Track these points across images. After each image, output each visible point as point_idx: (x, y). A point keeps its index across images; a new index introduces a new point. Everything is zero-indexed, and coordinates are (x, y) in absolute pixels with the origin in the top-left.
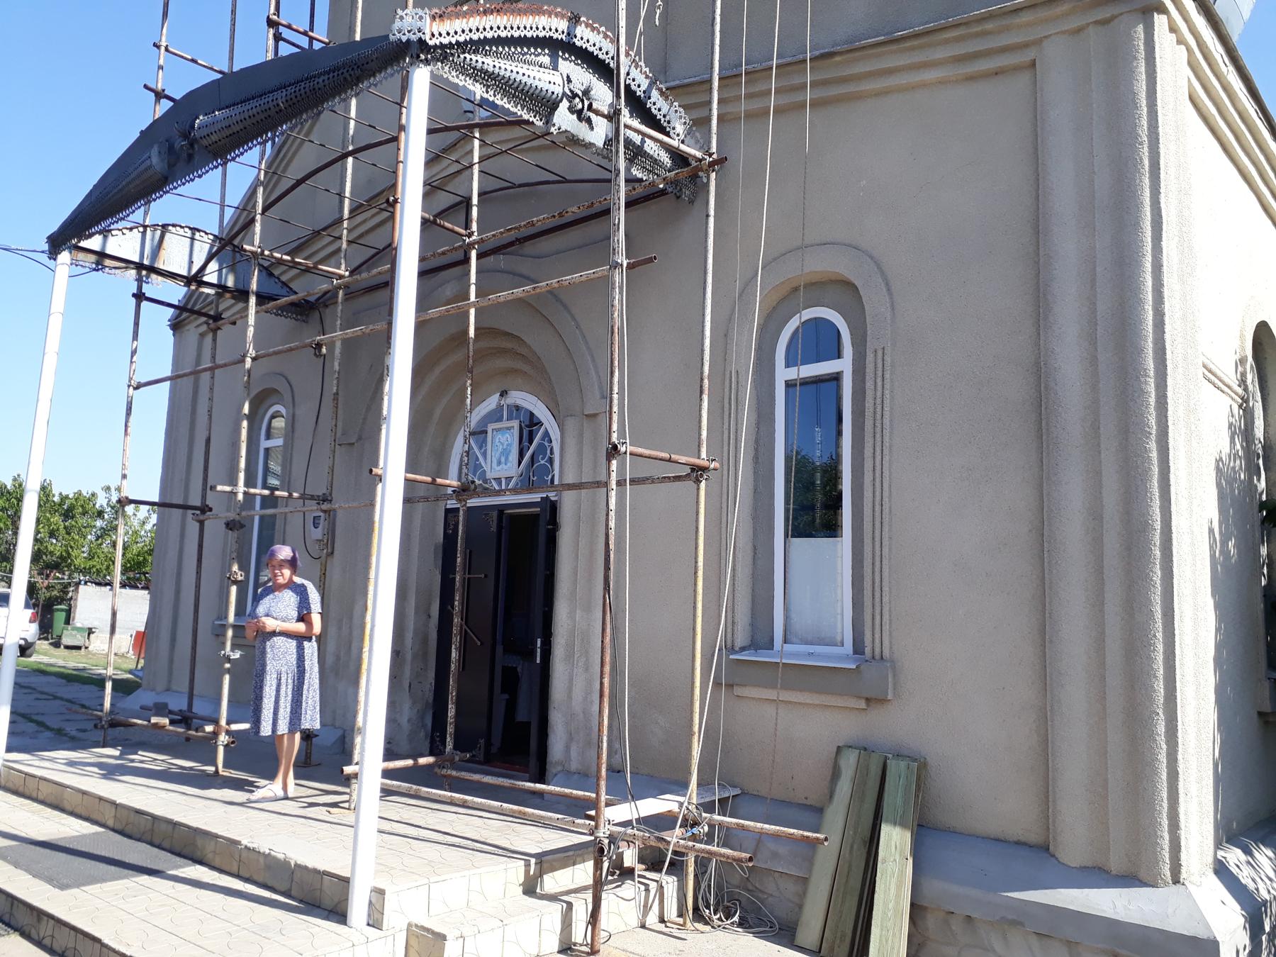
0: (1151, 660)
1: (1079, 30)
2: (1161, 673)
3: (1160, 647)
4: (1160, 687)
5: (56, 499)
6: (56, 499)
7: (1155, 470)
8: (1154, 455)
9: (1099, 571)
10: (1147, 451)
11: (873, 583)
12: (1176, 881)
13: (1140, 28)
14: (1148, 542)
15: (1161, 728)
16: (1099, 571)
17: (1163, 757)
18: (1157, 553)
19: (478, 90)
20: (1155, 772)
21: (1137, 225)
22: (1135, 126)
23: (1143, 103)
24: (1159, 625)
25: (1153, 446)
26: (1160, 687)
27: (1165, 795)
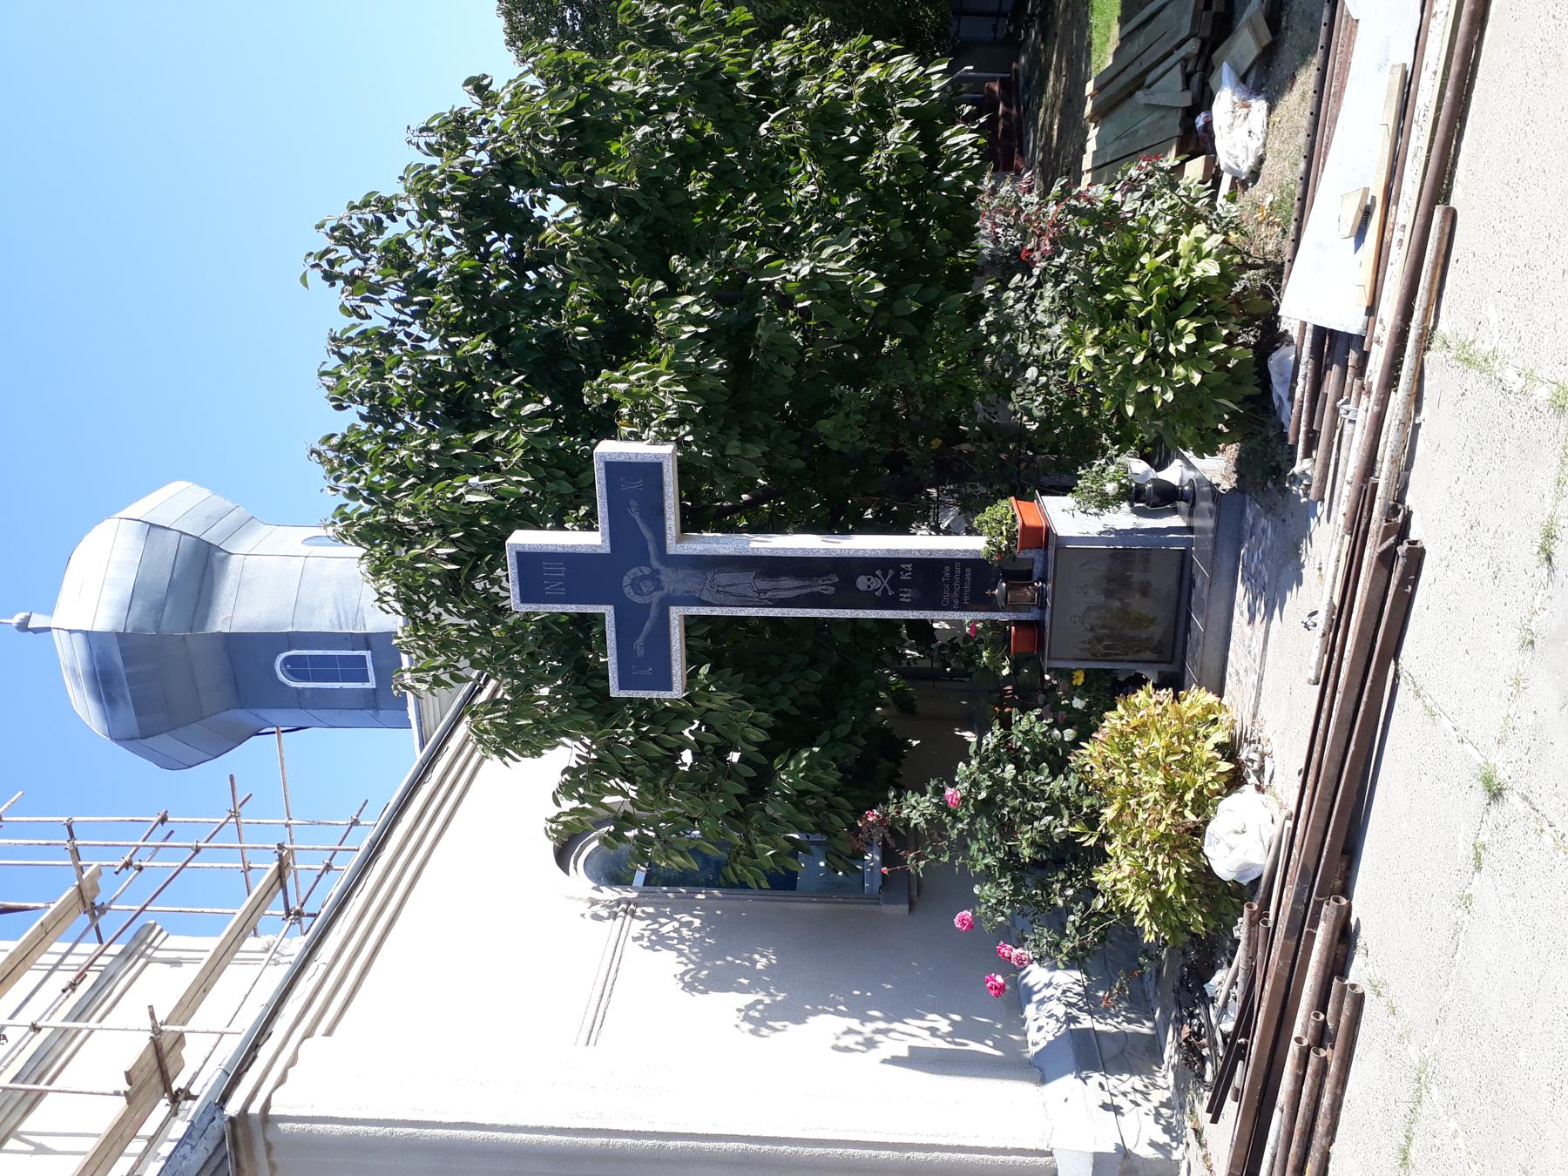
0: (861, 1158)
1: (273, 1166)
2: (873, 1153)
3: (850, 1151)
4: (884, 1154)
5: (353, 415)
6: (353, 415)
7: (693, 1144)
8: (679, 1143)
9: (1290, 1134)
10: (676, 1149)
11: (1339, 449)
12: (1050, 1154)
13: (281, 1126)
14: (757, 1153)
15: (920, 1155)
16: (1290, 1134)
17: (946, 1156)
18: (766, 1148)
19: (1293, 418)
20: (959, 1162)
21: (469, 1142)
22: (375, 1137)
23: (353, 1129)
24: (830, 1150)
25: (671, 1144)
26: (884, 1154)
27: (978, 1157)
